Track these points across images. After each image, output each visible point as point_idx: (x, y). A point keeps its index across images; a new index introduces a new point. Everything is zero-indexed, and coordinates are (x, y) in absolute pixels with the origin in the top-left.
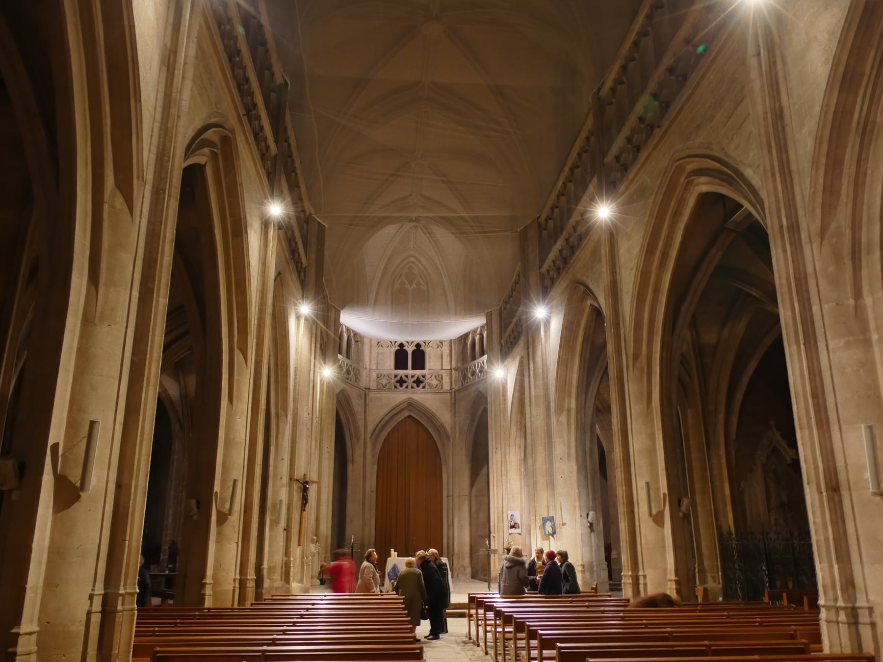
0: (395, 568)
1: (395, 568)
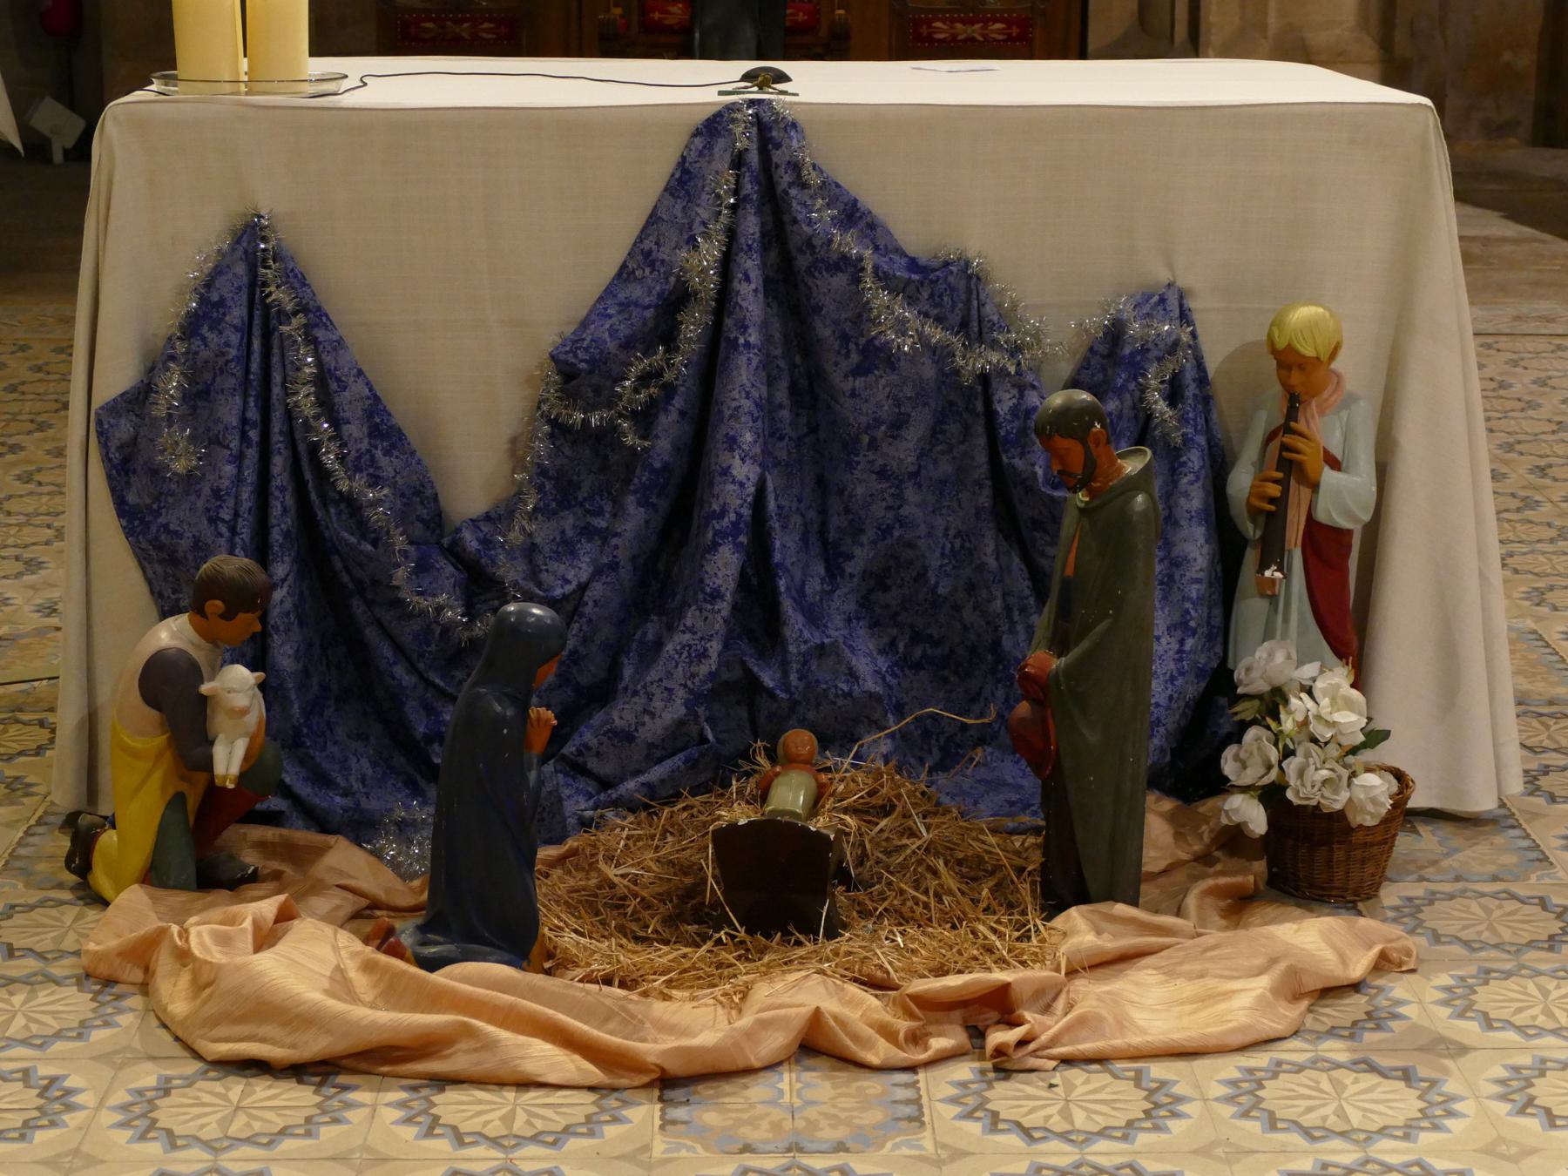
0: (255, 307)
1: (255, 307)
